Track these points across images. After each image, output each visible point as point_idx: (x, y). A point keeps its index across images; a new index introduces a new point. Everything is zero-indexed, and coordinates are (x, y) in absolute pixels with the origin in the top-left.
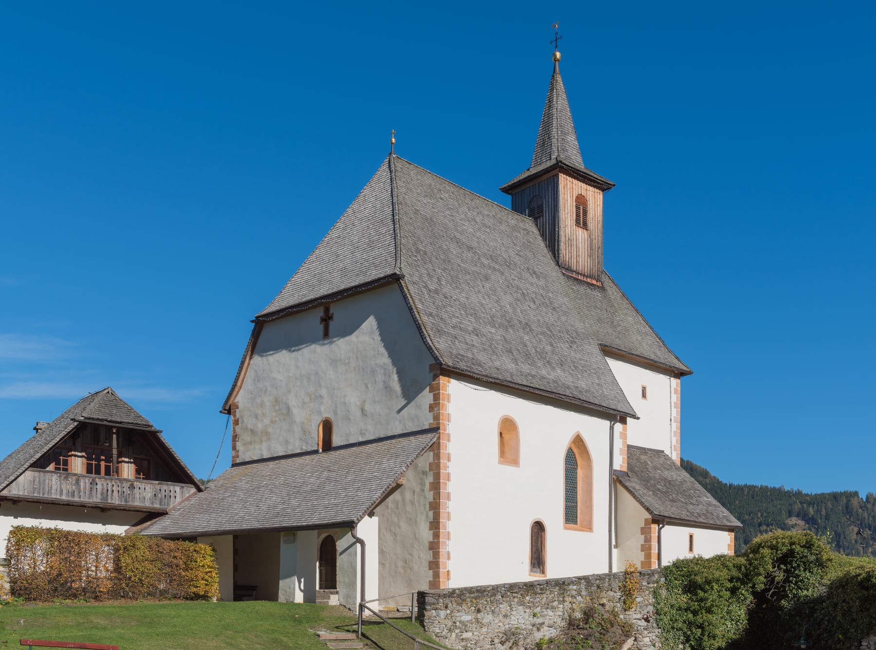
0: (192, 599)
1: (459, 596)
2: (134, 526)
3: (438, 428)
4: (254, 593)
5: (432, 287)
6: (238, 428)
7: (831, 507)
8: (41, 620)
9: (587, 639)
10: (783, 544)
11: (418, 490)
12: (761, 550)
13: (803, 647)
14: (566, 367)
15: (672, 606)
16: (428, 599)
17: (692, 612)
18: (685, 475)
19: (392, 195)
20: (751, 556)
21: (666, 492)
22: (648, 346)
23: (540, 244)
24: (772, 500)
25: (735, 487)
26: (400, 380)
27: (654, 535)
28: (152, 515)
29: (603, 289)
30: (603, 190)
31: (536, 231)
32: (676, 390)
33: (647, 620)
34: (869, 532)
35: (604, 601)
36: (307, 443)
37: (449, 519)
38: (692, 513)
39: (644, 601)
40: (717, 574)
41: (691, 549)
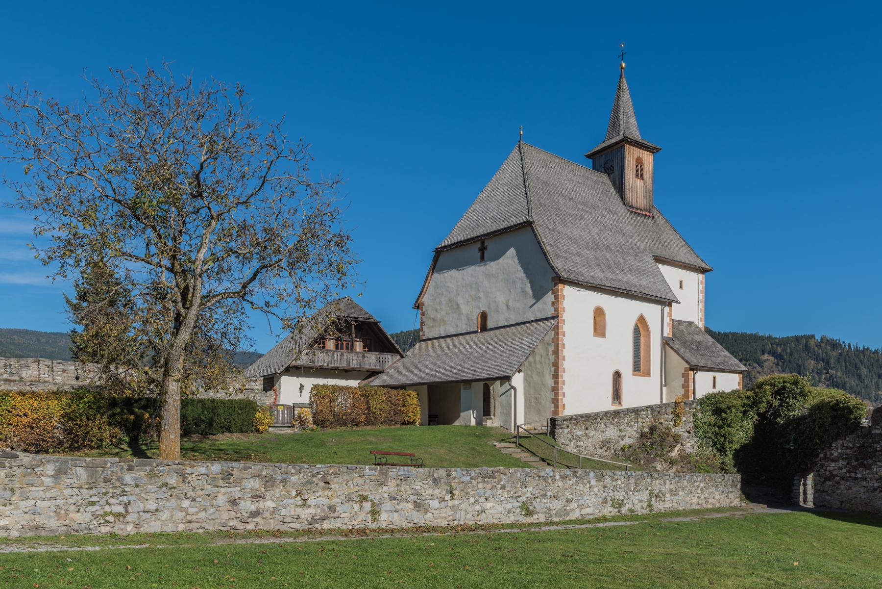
0: (405, 424)
1: (575, 420)
2: (363, 380)
3: (558, 316)
4: (436, 419)
5: (551, 227)
6: (424, 318)
7: (794, 346)
8: (342, 439)
9: (652, 445)
10: (779, 382)
11: (544, 354)
12: (764, 387)
13: (792, 448)
14: (633, 273)
15: (705, 423)
16: (558, 422)
17: (718, 427)
18: (708, 337)
19: (523, 169)
20: (757, 390)
21: (697, 350)
22: (684, 255)
23: (613, 191)
24: (750, 343)
25: (722, 334)
26: (532, 287)
27: (691, 378)
28: (373, 374)
29: (653, 217)
30: (653, 153)
31: (609, 183)
32: (701, 282)
33: (689, 432)
34: (823, 364)
35: (662, 421)
36: (470, 326)
37: (564, 372)
38: (715, 363)
39: (687, 421)
40: (735, 402)
41: (714, 386)
